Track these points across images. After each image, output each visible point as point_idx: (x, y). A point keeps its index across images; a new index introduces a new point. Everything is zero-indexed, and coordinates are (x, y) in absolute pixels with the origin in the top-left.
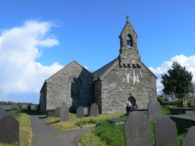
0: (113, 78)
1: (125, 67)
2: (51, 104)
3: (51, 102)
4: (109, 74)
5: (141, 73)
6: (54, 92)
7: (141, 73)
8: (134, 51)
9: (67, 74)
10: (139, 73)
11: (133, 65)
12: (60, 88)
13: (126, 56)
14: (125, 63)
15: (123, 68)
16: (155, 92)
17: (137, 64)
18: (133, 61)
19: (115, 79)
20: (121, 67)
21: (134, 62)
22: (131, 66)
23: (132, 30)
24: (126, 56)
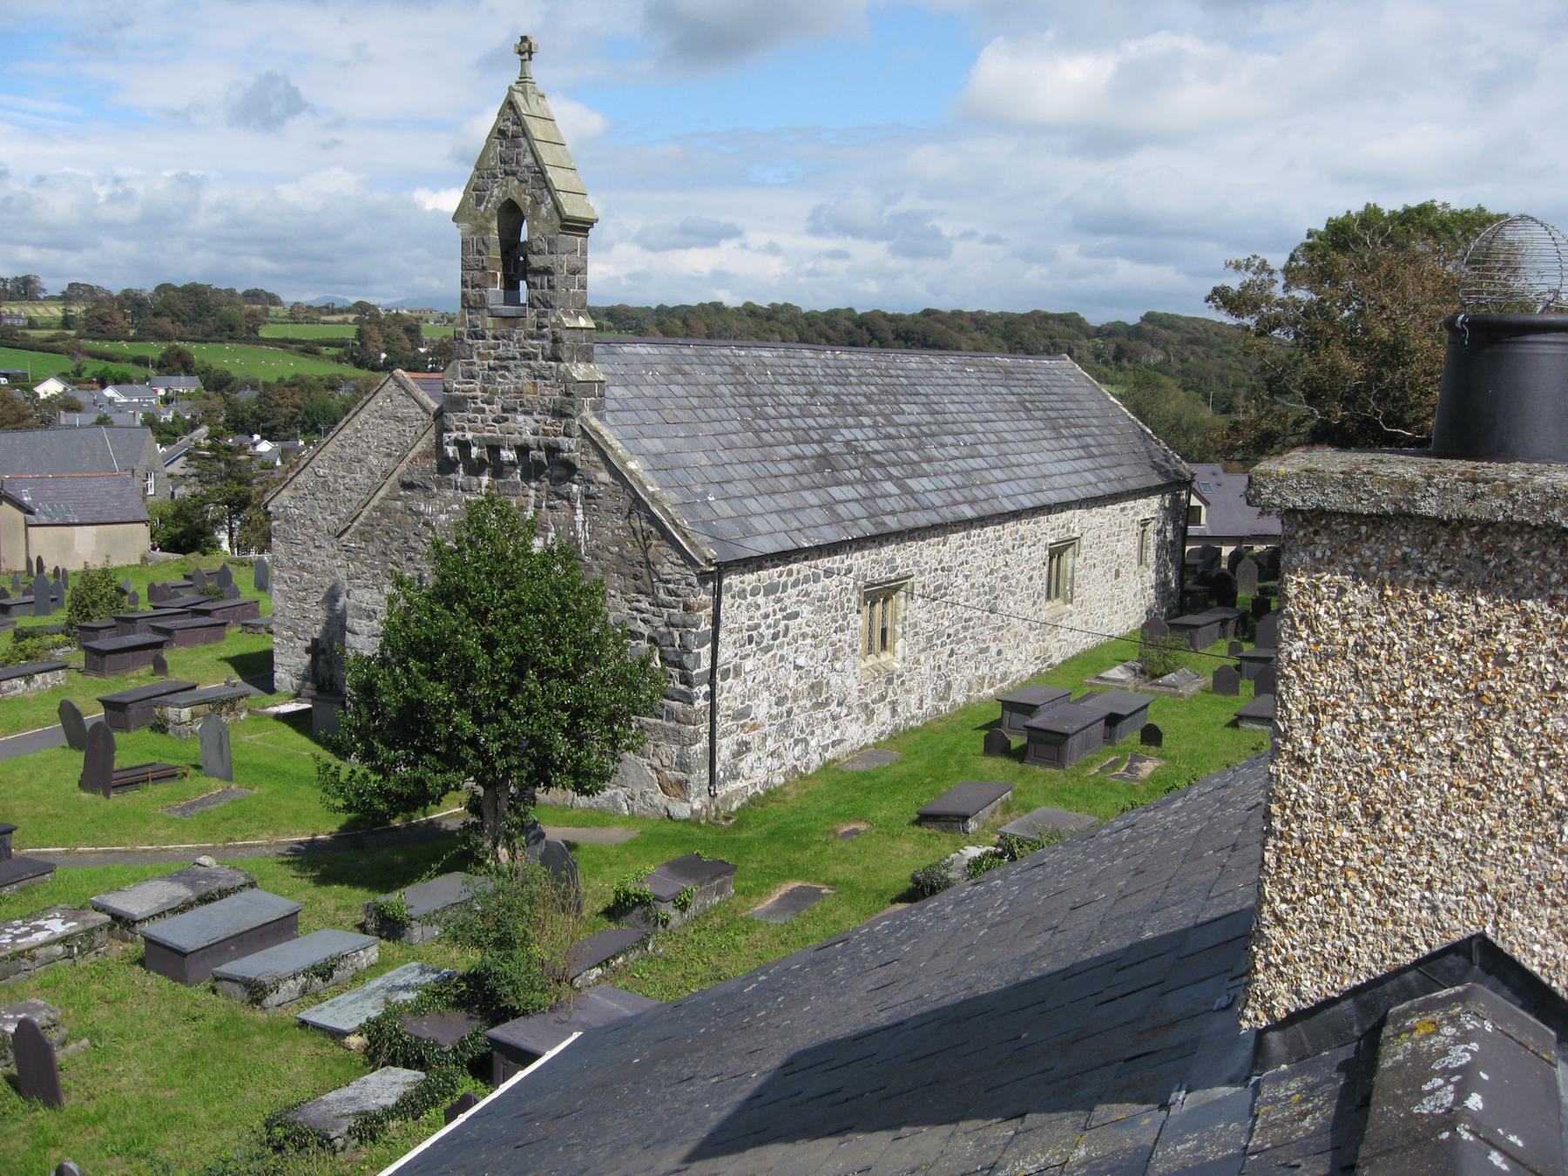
0: (406, 540)
1: (475, 468)
2: (290, 639)
3: (290, 628)
4: (384, 511)
5: (579, 517)
6: (302, 568)
7: (579, 517)
8: (531, 336)
9: (359, 461)
10: (562, 515)
11: (523, 450)
12: (331, 551)
13: (478, 383)
14: (469, 436)
15: (460, 476)
16: (676, 672)
17: (542, 439)
18: (520, 418)
19: (414, 549)
20: (447, 466)
21: (525, 427)
22: (508, 455)
23: (529, 160)
24: (478, 383)
